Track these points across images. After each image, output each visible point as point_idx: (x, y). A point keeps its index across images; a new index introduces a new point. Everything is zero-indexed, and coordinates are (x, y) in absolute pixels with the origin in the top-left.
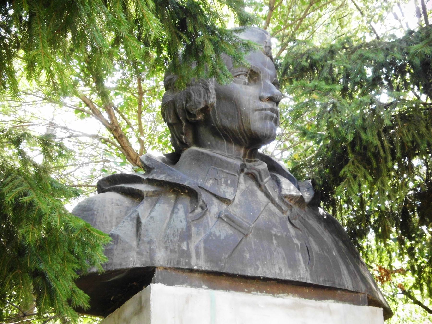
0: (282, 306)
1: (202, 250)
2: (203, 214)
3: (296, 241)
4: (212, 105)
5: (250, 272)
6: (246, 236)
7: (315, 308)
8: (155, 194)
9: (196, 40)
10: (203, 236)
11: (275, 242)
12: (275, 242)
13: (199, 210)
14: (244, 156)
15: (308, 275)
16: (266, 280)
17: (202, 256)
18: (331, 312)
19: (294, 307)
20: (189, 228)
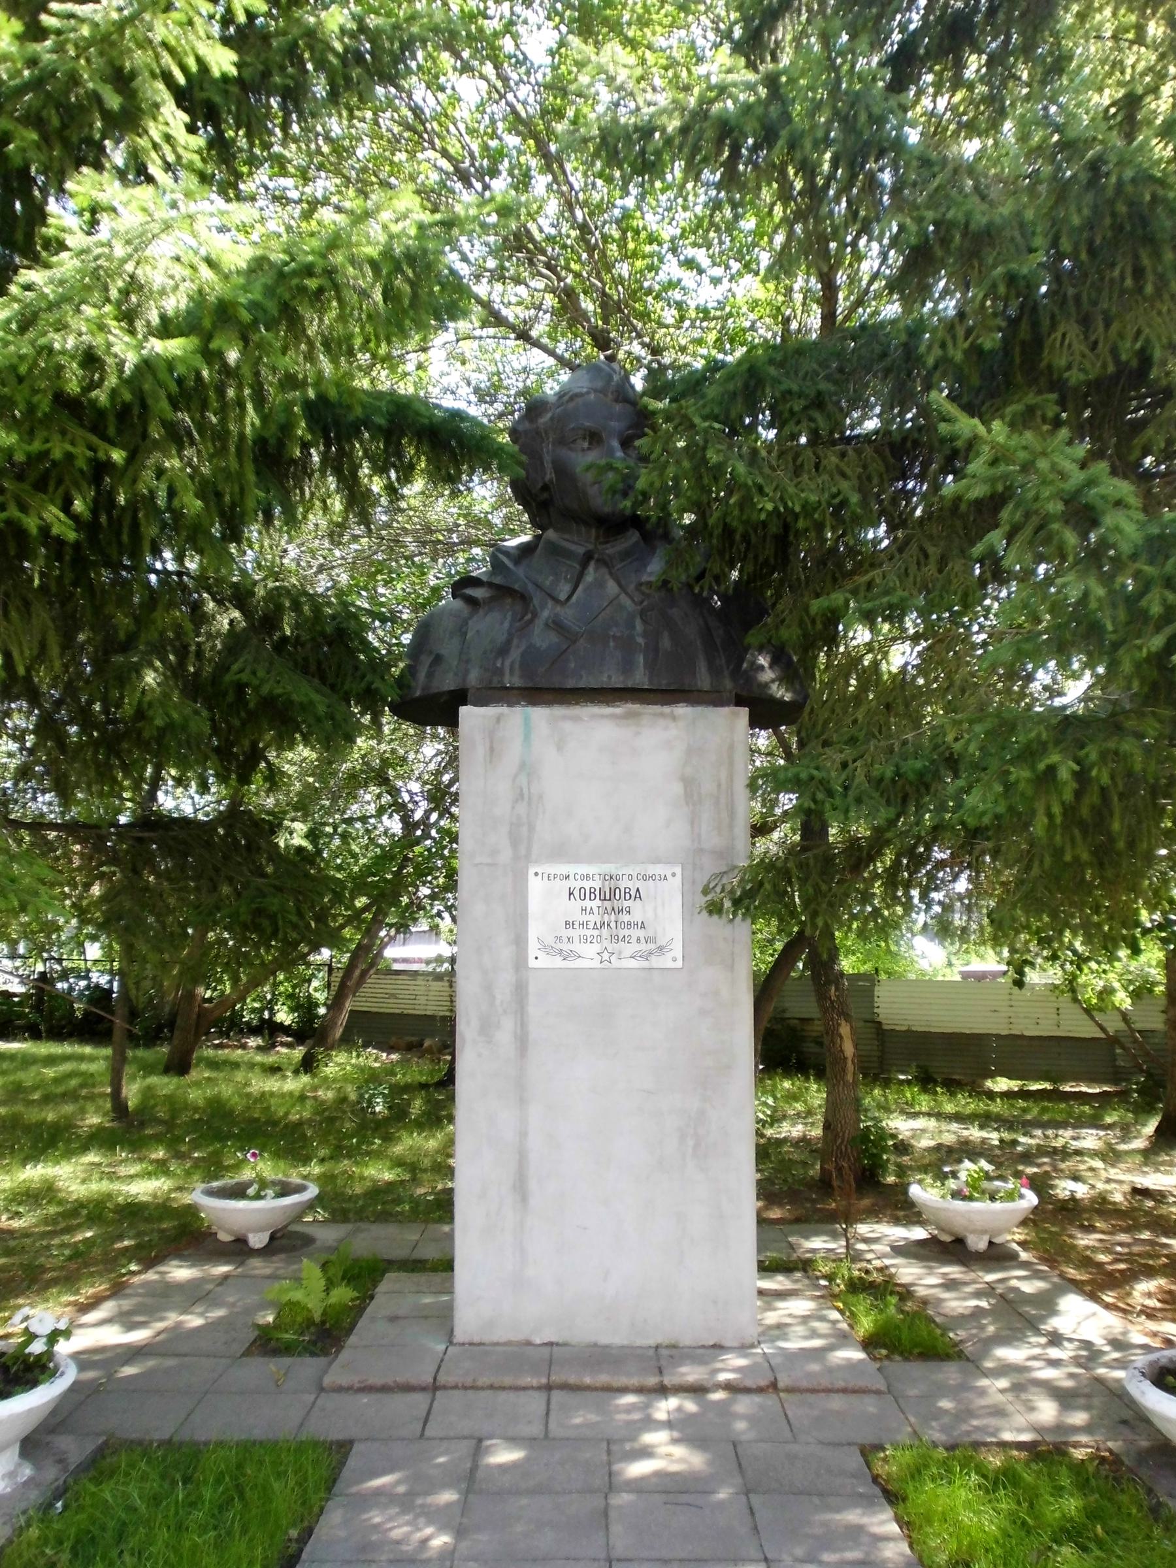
0: (613, 717)
1: (517, 666)
2: (531, 621)
3: (640, 640)
4: (551, 481)
5: (570, 683)
6: (574, 642)
7: (655, 715)
8: (492, 599)
9: (916, 154)
10: (523, 648)
11: (612, 644)
12: (612, 644)
13: (529, 616)
14: (597, 537)
15: (646, 680)
16: (615, 690)
17: (517, 672)
18: (674, 718)
19: (629, 716)
20: (509, 642)
